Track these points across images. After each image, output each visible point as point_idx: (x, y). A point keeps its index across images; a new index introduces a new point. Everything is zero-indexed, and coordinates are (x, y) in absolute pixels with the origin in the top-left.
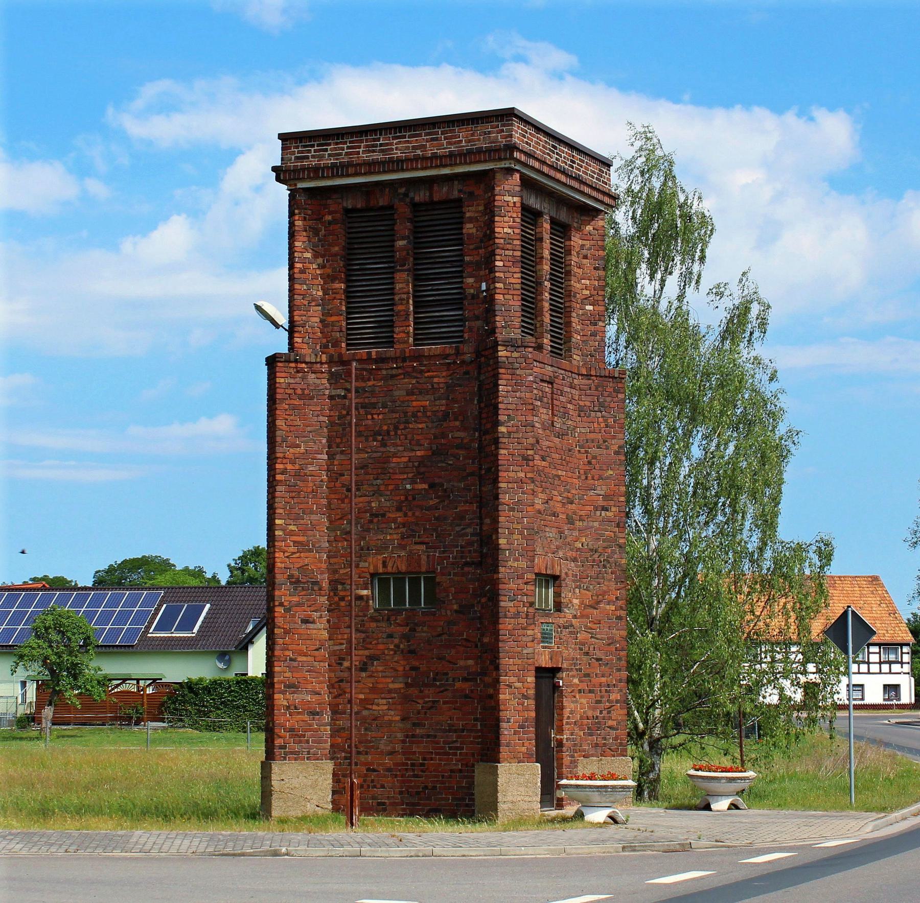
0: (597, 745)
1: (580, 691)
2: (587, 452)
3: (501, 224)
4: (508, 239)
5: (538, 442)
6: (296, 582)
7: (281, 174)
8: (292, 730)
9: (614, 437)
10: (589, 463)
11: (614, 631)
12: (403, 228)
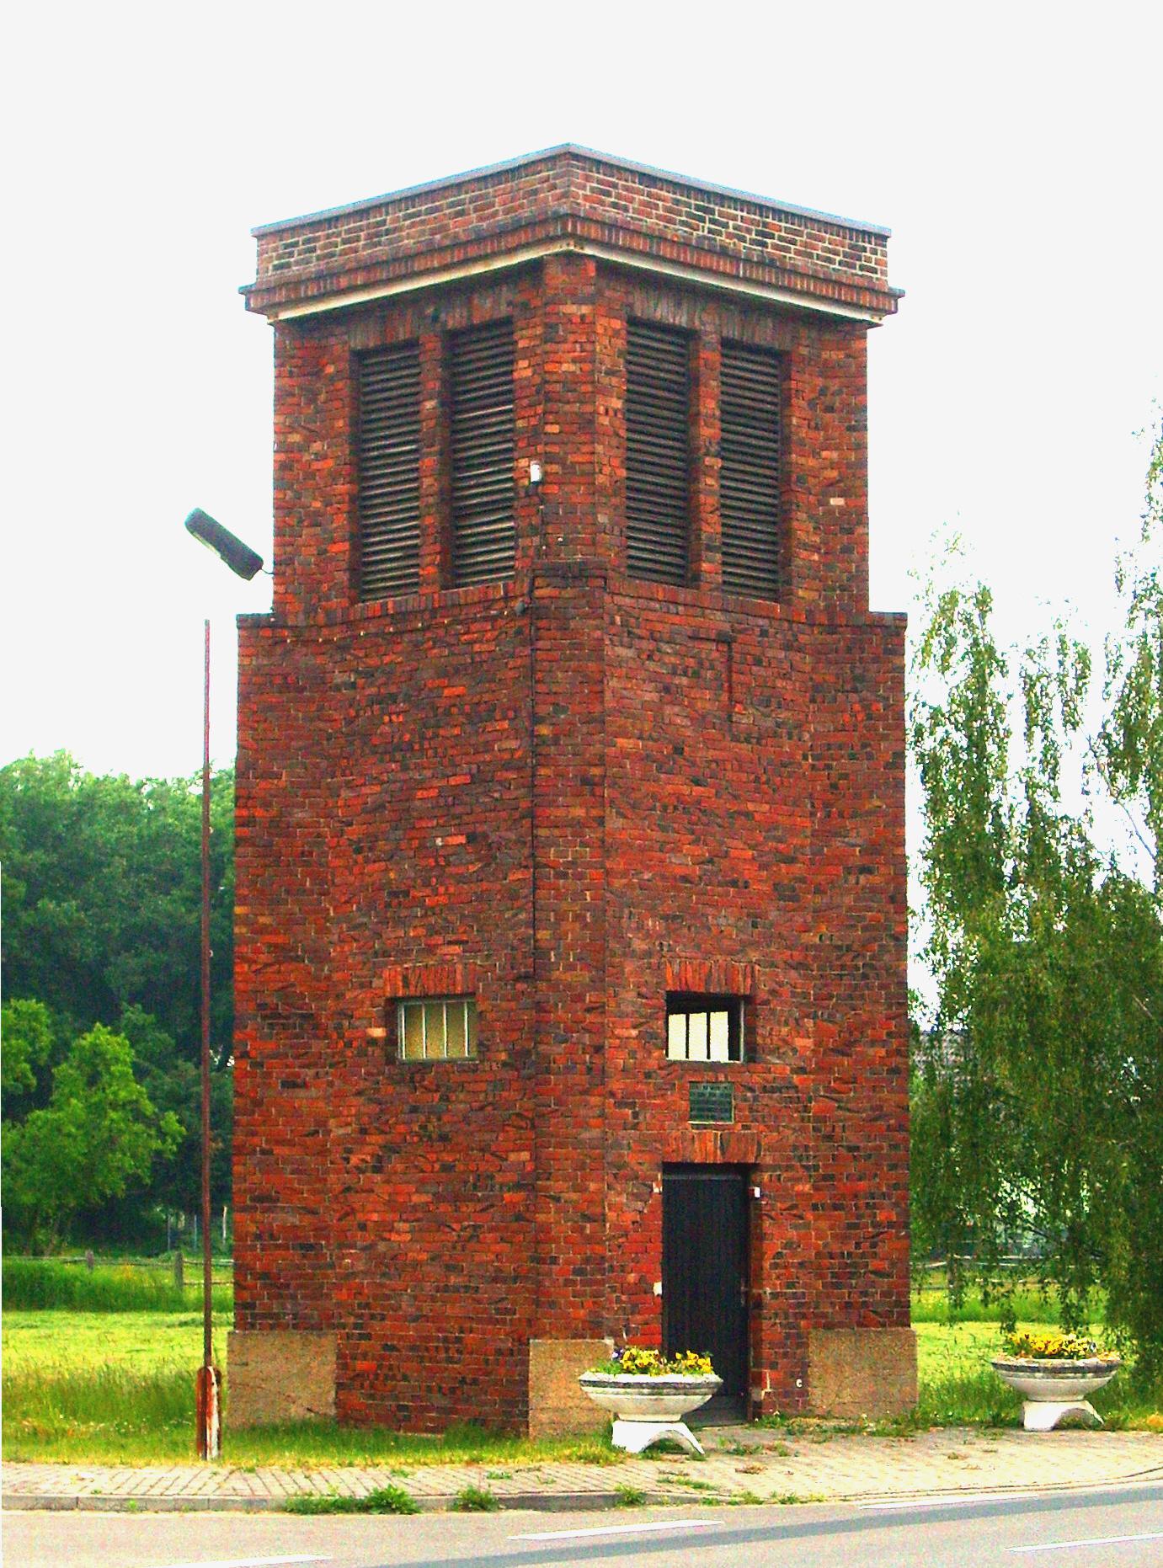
0: (847, 1306)
1: (815, 1207)
2: (829, 767)
5: (679, 750)
6: (271, 1015)
7: (262, 298)
8: (265, 1275)
11: (885, 1094)
12: (432, 378)
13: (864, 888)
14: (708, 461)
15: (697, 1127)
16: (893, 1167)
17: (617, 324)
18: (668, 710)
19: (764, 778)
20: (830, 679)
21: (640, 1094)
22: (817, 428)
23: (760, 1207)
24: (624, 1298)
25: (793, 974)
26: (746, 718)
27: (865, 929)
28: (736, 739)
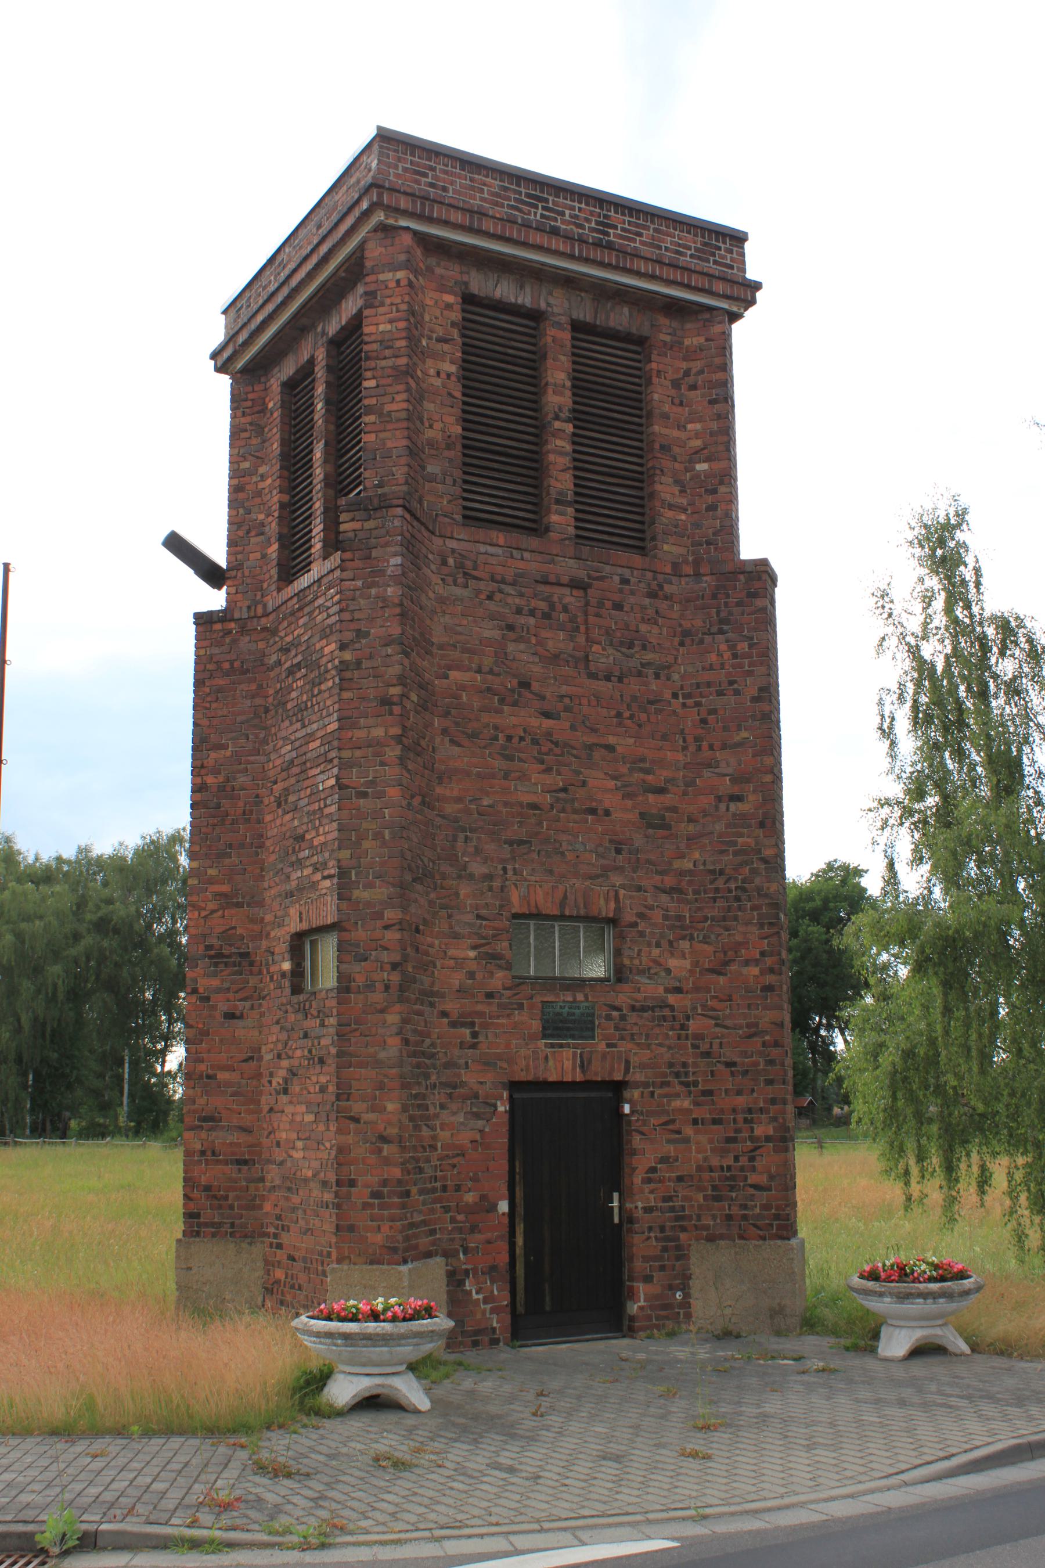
0: (729, 1217)
1: (695, 1122)
2: (698, 704)
3: (374, 320)
4: (386, 343)
5: (525, 685)
7: (219, 369)
8: (208, 1188)
9: (750, 673)
10: (704, 721)
13: (734, 815)
14: (557, 425)
15: (552, 1046)
16: (770, 1082)
17: (450, 299)
18: (511, 647)
19: (627, 714)
20: (698, 623)
21: (481, 1015)
22: (681, 404)
23: (629, 1122)
24: (460, 1217)
25: (664, 898)
26: (604, 657)
27: (736, 853)
28: (593, 676)
